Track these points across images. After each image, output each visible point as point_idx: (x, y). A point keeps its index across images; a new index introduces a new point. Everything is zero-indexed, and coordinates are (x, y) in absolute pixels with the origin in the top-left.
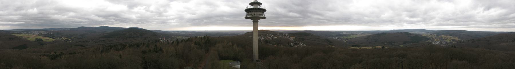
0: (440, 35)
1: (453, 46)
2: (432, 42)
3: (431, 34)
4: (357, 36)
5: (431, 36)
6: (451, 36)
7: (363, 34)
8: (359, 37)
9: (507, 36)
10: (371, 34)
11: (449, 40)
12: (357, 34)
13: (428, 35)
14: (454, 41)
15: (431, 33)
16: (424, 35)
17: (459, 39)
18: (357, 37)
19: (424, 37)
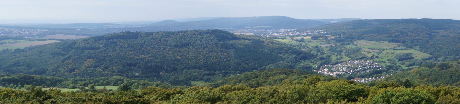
0: (350, 39)
1: (301, 62)
2: (319, 69)
3: (315, 38)
4: (22, 45)
5: (314, 44)
6: (396, 45)
7: (47, 37)
8: (29, 49)
9: (414, 77)
10: (79, 37)
11: (385, 59)
12: (21, 38)
13: (302, 40)
14: (408, 63)
15: (316, 32)
16: (287, 41)
17: (426, 55)
18: (22, 48)
19: (289, 50)
